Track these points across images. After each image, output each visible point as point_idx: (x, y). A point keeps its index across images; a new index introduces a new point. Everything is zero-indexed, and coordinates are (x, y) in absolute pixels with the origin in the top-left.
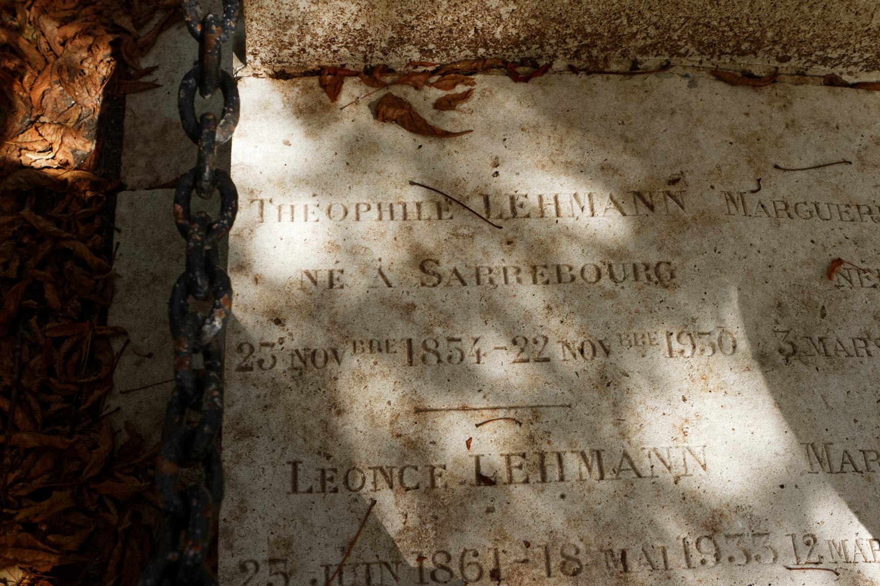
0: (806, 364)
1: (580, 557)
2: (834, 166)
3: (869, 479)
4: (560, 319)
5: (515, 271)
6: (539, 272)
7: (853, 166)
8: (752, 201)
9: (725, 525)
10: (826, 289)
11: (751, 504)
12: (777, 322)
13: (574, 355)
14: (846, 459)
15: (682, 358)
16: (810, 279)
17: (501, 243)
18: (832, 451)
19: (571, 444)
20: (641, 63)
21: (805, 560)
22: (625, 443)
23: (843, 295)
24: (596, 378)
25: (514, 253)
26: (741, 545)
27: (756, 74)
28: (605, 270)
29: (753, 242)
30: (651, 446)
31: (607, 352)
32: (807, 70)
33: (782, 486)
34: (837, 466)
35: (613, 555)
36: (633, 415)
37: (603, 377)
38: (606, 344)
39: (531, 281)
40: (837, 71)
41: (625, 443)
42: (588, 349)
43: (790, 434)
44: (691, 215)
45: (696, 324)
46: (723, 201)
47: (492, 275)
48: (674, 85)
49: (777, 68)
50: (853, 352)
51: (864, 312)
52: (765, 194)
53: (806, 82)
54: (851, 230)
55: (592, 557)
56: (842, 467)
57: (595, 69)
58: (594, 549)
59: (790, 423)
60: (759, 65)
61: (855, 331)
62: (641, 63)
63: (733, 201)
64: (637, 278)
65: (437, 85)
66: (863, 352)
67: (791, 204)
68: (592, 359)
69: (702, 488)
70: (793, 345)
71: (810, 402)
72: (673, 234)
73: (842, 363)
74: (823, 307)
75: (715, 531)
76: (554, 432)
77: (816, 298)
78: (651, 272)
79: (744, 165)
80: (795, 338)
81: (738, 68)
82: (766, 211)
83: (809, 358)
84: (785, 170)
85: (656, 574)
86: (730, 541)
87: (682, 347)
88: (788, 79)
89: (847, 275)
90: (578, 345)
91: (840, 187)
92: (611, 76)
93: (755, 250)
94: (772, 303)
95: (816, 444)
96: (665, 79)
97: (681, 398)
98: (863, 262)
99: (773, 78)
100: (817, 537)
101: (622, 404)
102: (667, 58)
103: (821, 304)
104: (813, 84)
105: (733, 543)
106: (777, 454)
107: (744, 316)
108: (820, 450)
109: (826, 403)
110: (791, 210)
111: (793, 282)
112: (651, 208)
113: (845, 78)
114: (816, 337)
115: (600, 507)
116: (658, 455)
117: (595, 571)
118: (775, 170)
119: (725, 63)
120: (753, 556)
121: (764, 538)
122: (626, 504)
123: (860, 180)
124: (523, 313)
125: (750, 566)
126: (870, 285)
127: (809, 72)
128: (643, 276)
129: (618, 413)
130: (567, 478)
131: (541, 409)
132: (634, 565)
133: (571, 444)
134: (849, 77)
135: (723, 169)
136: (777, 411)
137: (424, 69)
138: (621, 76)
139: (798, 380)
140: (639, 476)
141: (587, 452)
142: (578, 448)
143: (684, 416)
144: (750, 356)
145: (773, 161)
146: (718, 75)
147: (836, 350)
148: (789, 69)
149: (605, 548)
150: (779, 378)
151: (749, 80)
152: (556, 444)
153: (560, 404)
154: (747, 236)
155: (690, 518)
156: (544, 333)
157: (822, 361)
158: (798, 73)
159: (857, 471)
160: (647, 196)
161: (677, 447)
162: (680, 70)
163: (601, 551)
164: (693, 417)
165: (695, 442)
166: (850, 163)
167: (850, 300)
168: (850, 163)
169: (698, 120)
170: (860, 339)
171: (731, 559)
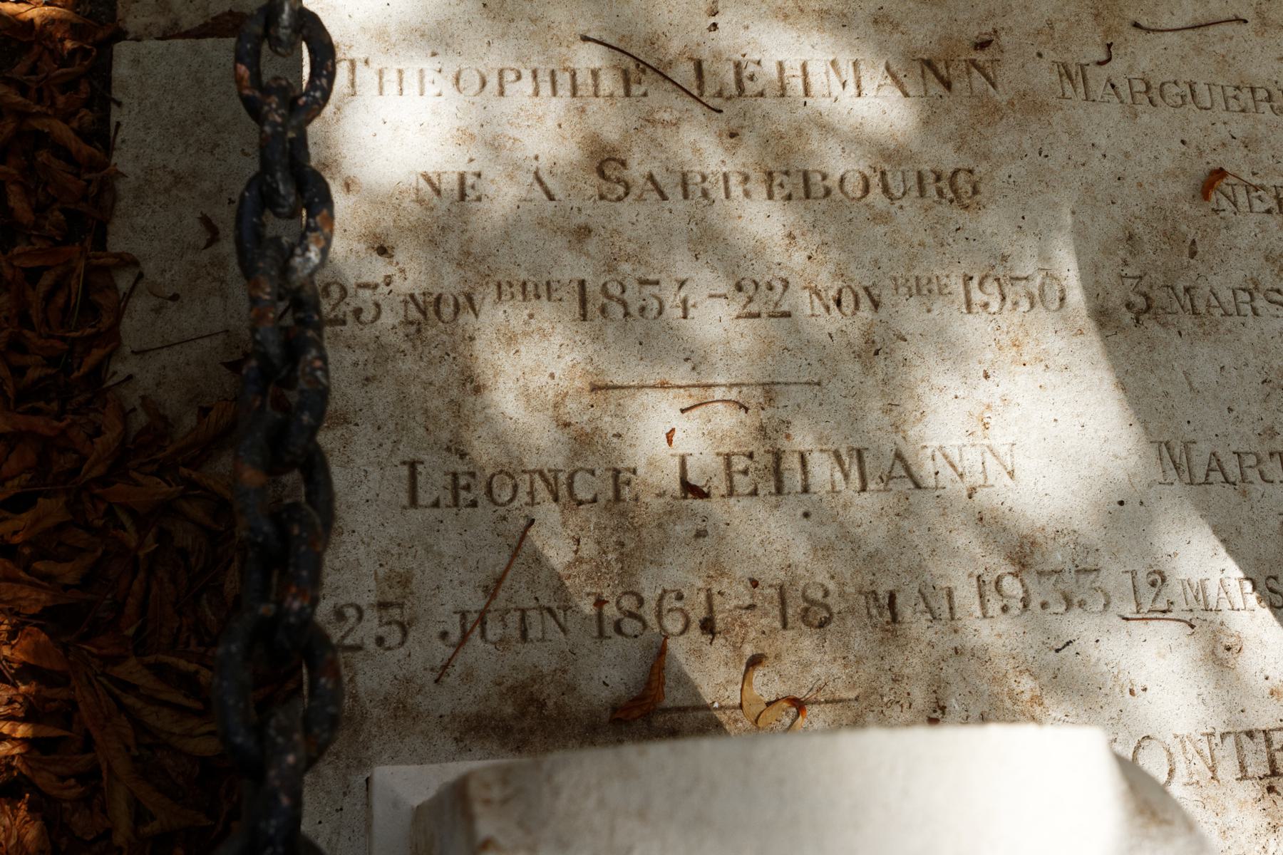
0: (1164, 325)
1: (829, 601)
4: (807, 253)
6: (777, 181)
7: (1248, 26)
8: (1098, 77)
9: (1038, 557)
11: (1076, 528)
13: (828, 309)
14: (1214, 464)
15: (985, 315)
16: (1176, 199)
21: (1149, 607)
23: (1223, 224)
25: (741, 151)
28: (875, 181)
29: (1096, 141)
33: (1121, 503)
34: (1200, 477)
35: (876, 599)
36: (912, 397)
38: (875, 292)
39: (765, 196)
42: (848, 300)
43: (1137, 428)
44: (1006, 98)
45: (1008, 265)
46: (1055, 77)
47: (706, 185)
50: (1232, 309)
51: (1252, 249)
52: (1118, 67)
54: (1240, 126)
55: (847, 601)
56: (1207, 475)
58: (850, 589)
61: (1237, 278)
63: (1070, 77)
66: (1246, 309)
67: (1155, 84)
68: (854, 314)
69: (1007, 504)
70: (1147, 297)
72: (979, 127)
73: (1217, 324)
74: (1194, 242)
77: (1184, 228)
78: (944, 184)
83: (1170, 318)
84: (1148, 30)
85: (938, 626)
86: (1044, 579)
87: (985, 298)
89: (1230, 194)
90: (832, 293)
93: (1098, 154)
95: (1172, 443)
98: (1254, 174)
100: (1166, 574)
101: (897, 381)
103: (1190, 237)
108: (1177, 451)
109: (1190, 384)
110: (1155, 94)
111: (1151, 203)
112: (948, 85)
115: (860, 530)
117: (850, 622)
118: (1133, 31)
120: (1075, 601)
121: (1092, 576)
125: (1070, 615)
128: (931, 191)
129: (889, 395)
130: (813, 489)
131: (777, 388)
132: (906, 613)
135: (1057, 26)
136: (1119, 394)
139: (1152, 349)
140: (918, 486)
141: (843, 452)
143: (986, 401)
145: (1132, 16)
147: (1209, 306)
150: (1124, 347)
153: (805, 380)
156: (783, 274)
157: (1188, 322)
160: (941, 66)
163: (860, 593)
164: (999, 402)
168: (1246, 22)
170: (1244, 290)
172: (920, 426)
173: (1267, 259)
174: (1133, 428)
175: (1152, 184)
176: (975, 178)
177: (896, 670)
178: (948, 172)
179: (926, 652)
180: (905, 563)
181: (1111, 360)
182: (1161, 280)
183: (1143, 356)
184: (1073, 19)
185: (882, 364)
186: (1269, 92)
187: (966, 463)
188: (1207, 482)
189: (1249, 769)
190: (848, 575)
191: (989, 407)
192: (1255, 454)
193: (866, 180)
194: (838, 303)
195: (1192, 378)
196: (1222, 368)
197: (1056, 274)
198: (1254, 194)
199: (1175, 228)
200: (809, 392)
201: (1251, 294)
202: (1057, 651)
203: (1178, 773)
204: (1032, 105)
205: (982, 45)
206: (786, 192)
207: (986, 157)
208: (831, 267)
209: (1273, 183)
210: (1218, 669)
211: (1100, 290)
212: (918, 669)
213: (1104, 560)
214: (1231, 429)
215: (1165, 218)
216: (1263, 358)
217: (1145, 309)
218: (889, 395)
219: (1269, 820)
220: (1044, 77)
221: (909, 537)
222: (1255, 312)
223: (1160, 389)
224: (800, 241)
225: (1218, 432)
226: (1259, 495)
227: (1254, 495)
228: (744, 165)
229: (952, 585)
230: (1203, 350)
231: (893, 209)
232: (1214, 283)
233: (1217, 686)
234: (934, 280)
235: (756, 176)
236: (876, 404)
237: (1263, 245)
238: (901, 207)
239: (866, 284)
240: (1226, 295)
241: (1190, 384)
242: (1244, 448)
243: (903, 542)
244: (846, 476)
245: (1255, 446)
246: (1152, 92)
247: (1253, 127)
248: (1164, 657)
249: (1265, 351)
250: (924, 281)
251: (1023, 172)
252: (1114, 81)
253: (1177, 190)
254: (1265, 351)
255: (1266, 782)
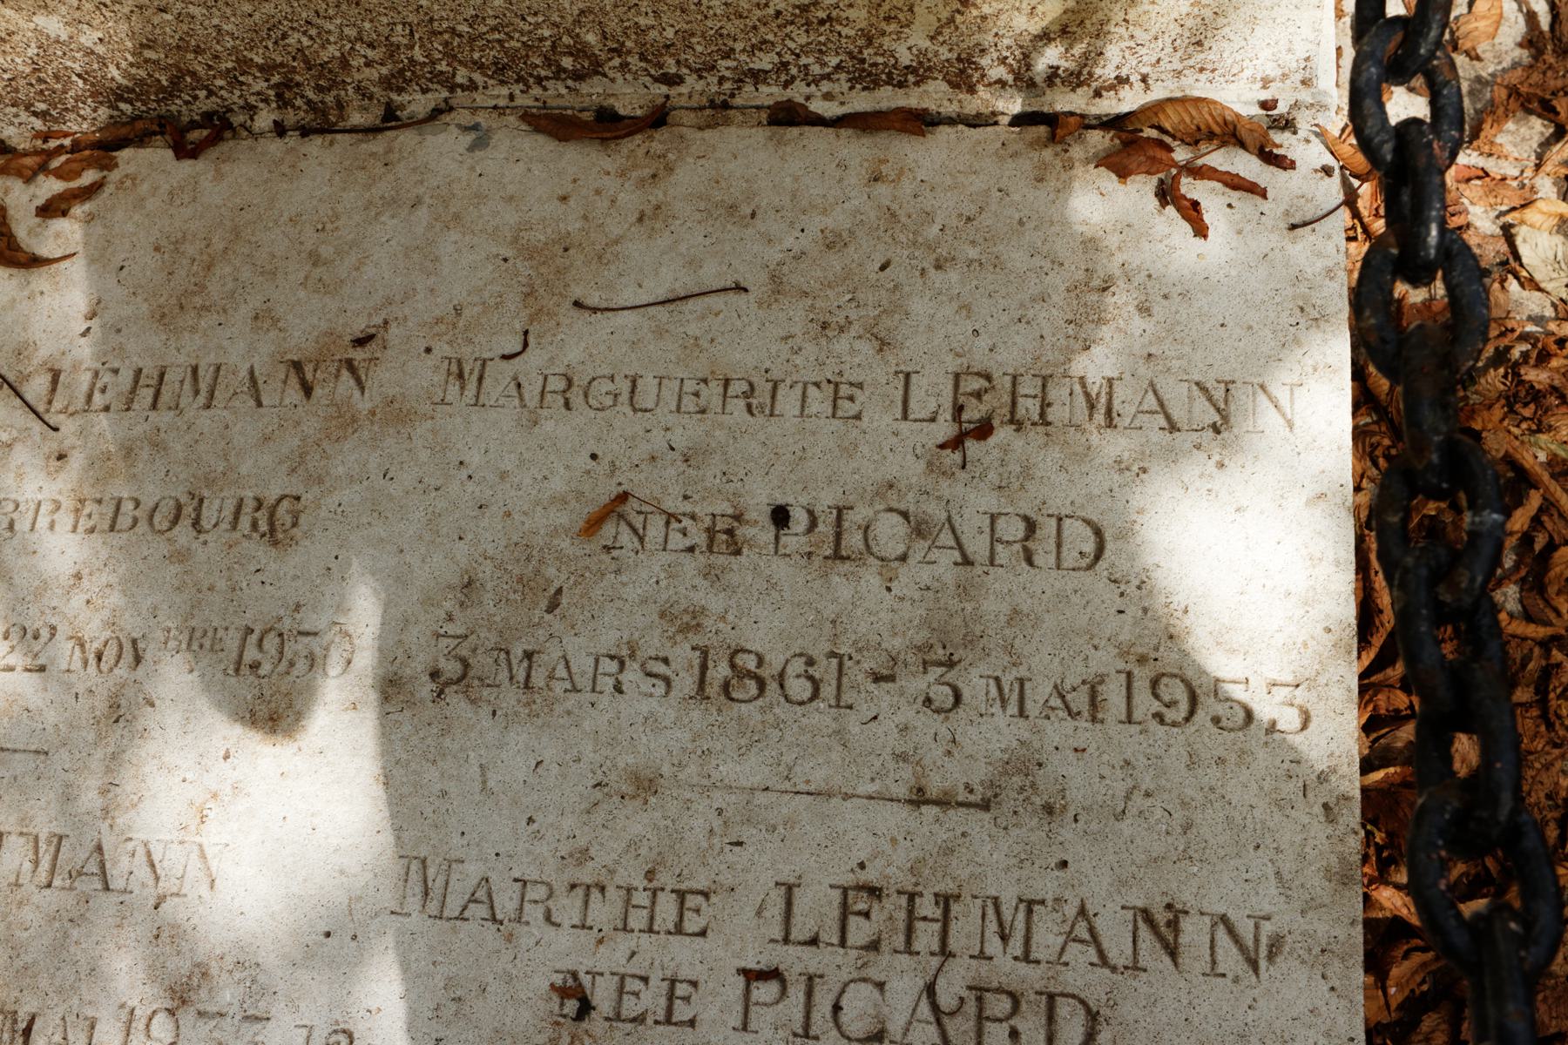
0: (473, 702)
2: (706, 299)
3: (510, 938)
5: (746, 517)
6: (86, 511)
7: (751, 297)
8: (501, 375)
9: (203, 994)
10: (580, 553)
11: (260, 961)
12: (450, 618)
13: (86, 663)
16: (555, 532)
20: (402, 107)
22: (104, 827)
23: (613, 567)
24: (101, 706)
25: (62, 475)
26: (216, 1034)
27: (622, 112)
28: (188, 510)
30: (142, 836)
31: (138, 659)
32: (732, 96)
33: (328, 935)
34: (453, 907)
35: (15, 1021)
38: (141, 645)
40: (798, 92)
41: (104, 827)
42: (110, 654)
43: (388, 838)
44: (369, 405)
45: (298, 616)
46: (439, 378)
47: (15, 516)
48: (443, 149)
49: (667, 97)
50: (584, 682)
51: (644, 601)
52: (534, 359)
53: (727, 122)
54: (686, 432)
56: (465, 908)
57: (321, 125)
60: (629, 96)
61: (608, 640)
62: (402, 107)
63: (461, 376)
64: (234, 525)
65: (60, 174)
66: (607, 684)
67: (580, 380)
68: (111, 670)
70: (466, 665)
71: (451, 777)
72: (325, 444)
73: (550, 705)
74: (559, 591)
75: (184, 1002)
77: (551, 572)
78: (262, 517)
79: (513, 301)
80: (474, 650)
81: (587, 102)
82: (521, 398)
83: (486, 692)
84: (595, 310)
86: (200, 1023)
87: (259, 656)
88: (689, 118)
89: (639, 526)
90: (96, 645)
91: (704, 343)
92: (339, 136)
93: (464, 473)
95: (429, 862)
96: (429, 137)
97: (222, 753)
98: (686, 497)
99: (658, 118)
100: (356, 1036)
101: (126, 756)
102: (445, 94)
103: (556, 585)
104: (740, 126)
106: (342, 872)
108: (431, 872)
109: (484, 782)
110: (576, 397)
111: (515, 539)
112: (307, 390)
113: (818, 106)
114: (517, 652)
115: (26, 934)
116: (149, 854)
118: (575, 313)
119: (560, 96)
121: (259, 1026)
123: (754, 327)
124: (37, 583)
126: (681, 547)
127: (738, 101)
134: (827, 104)
135: (467, 313)
136: (378, 791)
137: (58, 142)
138: (360, 136)
139: (444, 733)
140: (107, 889)
141: (43, 837)
142: (31, 829)
143: (214, 787)
144: (370, 681)
145: (577, 292)
146: (557, 126)
147: (551, 677)
148: (696, 97)
150: (407, 728)
151: (607, 126)
153: (33, 748)
154: (459, 446)
156: (53, 621)
157: (510, 698)
158: (712, 104)
159: (494, 919)
160: (308, 370)
161: (181, 843)
162: (464, 117)
164: (228, 790)
165: (212, 836)
166: (746, 290)
167: (624, 578)
168: (746, 290)
169: (457, 217)
170: (612, 657)
172: (132, 813)
173: (662, 615)
175: (525, 513)
176: (300, 506)
181: (383, 744)
182: (493, 638)
184: (492, 302)
185: (119, 732)
186: (751, 385)
188: (461, 918)
191: (215, 796)
192: (548, 884)
193: (179, 508)
194: (99, 658)
195: (489, 775)
198: (674, 525)
199: (537, 572)
200: (30, 762)
201: (622, 664)
204: (397, 414)
205: (361, 342)
207: (320, 481)
208: (106, 613)
209: (710, 510)
211: (400, 653)
213: (278, 1009)
216: (604, 752)
218: (112, 771)
220: (425, 375)
222: (618, 689)
223: (438, 787)
225: (501, 850)
226: (532, 941)
232: (569, 648)
234: (210, 634)
238: (205, 543)
239: (135, 635)
240: (582, 664)
242: (532, 873)
245: (550, 874)
246: (569, 390)
247: (707, 434)
249: (613, 743)
251: (357, 498)
252: (522, 379)
253: (558, 522)
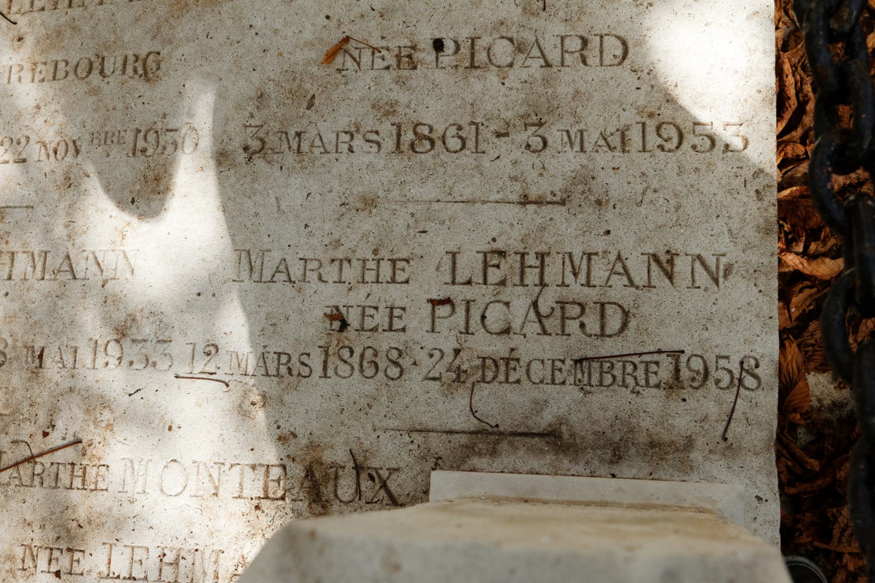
0: (269, 162)
1: (7, 351)
4: (44, 118)
5: (418, 47)
6: (38, 70)
9: (134, 330)
12: (252, 116)
13: (48, 156)
14: (282, 268)
15: (143, 157)
16: (308, 63)
17: (13, 40)
18: (266, 260)
19: (24, 244)
21: (200, 370)
23: (344, 81)
25: (22, 50)
28: (96, 65)
29: (254, 24)
30: (91, 249)
33: (199, 294)
34: (267, 275)
35: (33, 352)
36: (83, 216)
37: (67, 179)
38: (78, 143)
39: (30, 80)
41: (69, 245)
42: (61, 150)
43: (227, 240)
45: (165, 121)
50: (331, 148)
55: (16, 351)
56: (273, 276)
58: (19, 344)
59: (230, 228)
61: (343, 123)
68: (63, 158)
69: (124, 292)
72: (171, 20)
73: (313, 161)
74: (313, 97)
75: (124, 335)
76: (13, 233)
77: (308, 86)
80: (267, 133)
83: (276, 157)
85: (63, 372)
86: (134, 345)
87: (145, 145)
90: (53, 145)
93: (253, 32)
94: (253, 94)
98: (383, 38)
100: (219, 347)
101: (77, 206)
103: (311, 93)
105: (137, 348)
107: (216, 110)
108: (253, 257)
109: (279, 207)
111: (286, 68)
114: (292, 132)
115: (33, 305)
116: (96, 258)
117: (15, 365)
120: (150, 361)
121: (166, 345)
122: (55, 304)
124: (15, 113)
125: (145, 372)
126: (382, 67)
128: (130, 70)
129: (70, 214)
130: (13, 277)
131: (7, 210)
132: (47, 362)
133: (24, 244)
136: (220, 215)
139: (254, 181)
140: (75, 278)
141: (36, 253)
147: (312, 146)
149: (28, 345)
150: (233, 180)
152: (12, 244)
153: (25, 205)
155: (107, 319)
156: (27, 134)
157: (290, 159)
159: (290, 281)
161: (113, 251)
163: (25, 347)
167: (350, 87)
170: (346, 133)
171: (131, 363)
172: (84, 236)
173: (373, 107)
174: (223, 240)
176: (160, 58)
177: (33, 398)
178: (144, 56)
179: (53, 388)
180: (54, 329)
182: (277, 126)
183: (246, 186)
187: (106, 262)
189: (244, 491)
190: (20, 335)
192: (319, 260)
193: (91, 64)
195: (281, 202)
196: (308, 195)
197: (196, 126)
199: (300, 87)
200: (24, 213)
201: (352, 136)
202: (130, 395)
203: (188, 488)
206: (42, 76)
207: (170, 42)
208: (57, 127)
209: (397, 44)
210: (240, 417)
211: (225, 138)
212: (46, 399)
213: (176, 335)
214: (303, 240)
215: (294, 79)
217: (258, 150)
218: (70, 214)
219: (250, 529)
221: (60, 312)
222: (351, 150)
223: (253, 211)
224: (43, 110)
225: (291, 243)
226: (312, 292)
227: (307, 291)
228: (22, 60)
229: (78, 345)
230: (296, 181)
231: (103, 85)
232: (322, 129)
233: (237, 430)
234: (117, 134)
235: (27, 66)
236: (62, 220)
237: (374, 96)
238: (108, 83)
239: (74, 138)
241: (279, 207)
242: (309, 255)
243: (56, 315)
244: (34, 267)
245: (320, 255)
248: (200, 406)
250: (110, 135)
251: (193, 51)
254: (350, 180)
255: (255, 502)
